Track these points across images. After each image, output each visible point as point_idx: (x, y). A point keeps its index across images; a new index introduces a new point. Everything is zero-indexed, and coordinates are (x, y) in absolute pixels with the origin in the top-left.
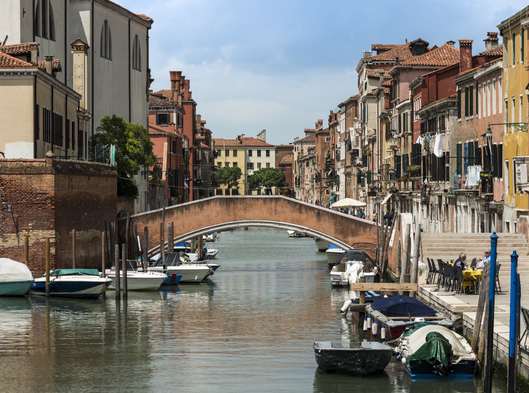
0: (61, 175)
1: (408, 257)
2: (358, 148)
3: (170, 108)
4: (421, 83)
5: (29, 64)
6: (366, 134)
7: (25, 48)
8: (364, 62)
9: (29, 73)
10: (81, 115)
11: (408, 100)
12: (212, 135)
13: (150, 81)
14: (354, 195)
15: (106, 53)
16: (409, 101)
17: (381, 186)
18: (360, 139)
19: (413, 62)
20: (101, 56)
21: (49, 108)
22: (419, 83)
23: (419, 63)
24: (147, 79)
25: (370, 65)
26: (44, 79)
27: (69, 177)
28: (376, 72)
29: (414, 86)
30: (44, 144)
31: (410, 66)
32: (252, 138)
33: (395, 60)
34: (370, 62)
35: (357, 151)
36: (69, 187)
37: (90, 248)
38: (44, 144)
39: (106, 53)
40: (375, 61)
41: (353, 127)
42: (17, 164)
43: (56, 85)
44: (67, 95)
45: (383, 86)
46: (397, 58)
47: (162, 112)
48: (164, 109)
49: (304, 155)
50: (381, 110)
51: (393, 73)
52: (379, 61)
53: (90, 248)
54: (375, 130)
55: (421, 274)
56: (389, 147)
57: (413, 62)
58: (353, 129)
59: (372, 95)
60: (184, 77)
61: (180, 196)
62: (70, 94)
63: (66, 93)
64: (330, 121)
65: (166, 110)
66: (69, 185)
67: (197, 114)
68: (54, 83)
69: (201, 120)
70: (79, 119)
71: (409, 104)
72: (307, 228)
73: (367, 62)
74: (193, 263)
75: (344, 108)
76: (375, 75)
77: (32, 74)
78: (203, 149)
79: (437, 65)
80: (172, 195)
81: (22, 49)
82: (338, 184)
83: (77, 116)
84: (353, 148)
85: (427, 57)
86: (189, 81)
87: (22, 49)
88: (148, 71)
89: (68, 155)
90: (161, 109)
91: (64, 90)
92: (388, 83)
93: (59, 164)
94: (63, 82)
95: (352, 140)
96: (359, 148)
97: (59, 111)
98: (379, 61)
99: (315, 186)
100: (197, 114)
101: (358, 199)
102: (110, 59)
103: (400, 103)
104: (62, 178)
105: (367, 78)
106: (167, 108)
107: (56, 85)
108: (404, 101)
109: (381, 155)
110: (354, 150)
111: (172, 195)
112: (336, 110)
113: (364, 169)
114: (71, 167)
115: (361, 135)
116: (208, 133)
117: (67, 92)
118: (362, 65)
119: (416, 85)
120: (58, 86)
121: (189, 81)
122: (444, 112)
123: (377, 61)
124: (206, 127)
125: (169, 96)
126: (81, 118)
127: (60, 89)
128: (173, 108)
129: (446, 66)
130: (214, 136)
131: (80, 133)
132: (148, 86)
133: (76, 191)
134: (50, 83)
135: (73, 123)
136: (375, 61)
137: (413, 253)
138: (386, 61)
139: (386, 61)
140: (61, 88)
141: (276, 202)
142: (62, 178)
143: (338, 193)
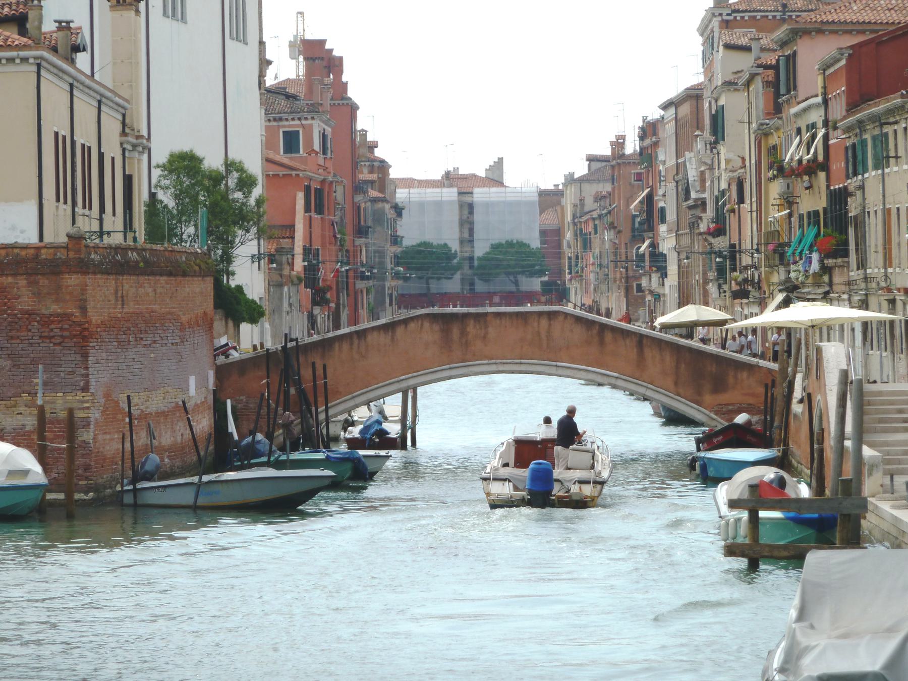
0: (99, 276)
1: (841, 436)
2: (703, 196)
3: (306, 119)
4: (843, 62)
5: (25, 40)
6: (723, 165)
7: (14, 7)
8: (713, 14)
9: (25, 60)
10: (128, 142)
11: (816, 96)
12: (391, 171)
13: (265, 63)
14: (697, 294)
15: (174, 9)
16: (819, 99)
17: (759, 276)
18: (708, 176)
19: (824, 17)
20: (165, 14)
21: (65, 131)
22: (839, 60)
23: (835, 17)
24: (260, 59)
25: (727, 22)
26: (55, 71)
27: (116, 280)
28: (741, 37)
29: (829, 67)
30: (57, 207)
31: (817, 26)
32: (474, 176)
33: (780, 8)
34: (728, 15)
35: (704, 203)
36: (117, 300)
37: (163, 427)
38: (57, 207)
39: (174, 9)
40: (738, 11)
41: (691, 150)
42: (7, 255)
43: (78, 81)
44: (100, 102)
45: (759, 66)
46: (784, 6)
47: (289, 126)
48: (293, 119)
49: (586, 209)
50: (758, 117)
51: (781, 40)
52: (746, 11)
53: (163, 427)
54: (743, 159)
55: (870, 474)
56: (777, 197)
57: (829, 17)
58: (692, 154)
59: (736, 84)
60: (331, 50)
61: (333, 305)
62: (107, 98)
63: (99, 98)
64: (642, 138)
65: (297, 122)
66: (116, 297)
67: (359, 128)
68: (75, 79)
69: (368, 139)
70: (124, 150)
71: (817, 105)
72: (616, 375)
73: (721, 15)
74: (644, 547)
75: (672, 111)
76: (740, 43)
77: (31, 61)
78: (374, 200)
79: (875, 23)
80: (315, 303)
81: (6, 10)
82: (664, 275)
83: (121, 144)
84: (693, 195)
85: (853, 5)
86: (341, 59)
87: (6, 10)
88: (262, 43)
89: (105, 229)
90: (287, 120)
91: (94, 91)
92: (771, 59)
93: (96, 252)
94: (89, 73)
95: (691, 179)
96: (706, 195)
97: (85, 136)
98: (746, 11)
99: (611, 276)
100: (359, 128)
101: (706, 304)
102: (183, 19)
103: (799, 103)
104: (101, 282)
105: (721, 48)
106: (299, 119)
107: (78, 81)
108: (807, 99)
109: (759, 211)
110: (696, 200)
111: (315, 303)
112: (655, 113)
113: (720, 243)
114: (119, 257)
115: (712, 168)
116: (383, 167)
117: (102, 95)
118: (710, 21)
119: (832, 65)
120: (82, 84)
121: (341, 59)
122: (896, 123)
123: (743, 11)
124: (378, 153)
125: (301, 91)
126: (129, 147)
127: (87, 90)
128: (313, 118)
129: (899, 23)
130: (394, 174)
131: (128, 181)
132: (262, 75)
133: (130, 308)
134: (66, 77)
135: (64, 137)
136: (738, 11)
137: (849, 428)
138: (760, 11)
139: (760, 11)
140: (89, 88)
141: (550, 319)
142: (101, 282)
143: (661, 291)
